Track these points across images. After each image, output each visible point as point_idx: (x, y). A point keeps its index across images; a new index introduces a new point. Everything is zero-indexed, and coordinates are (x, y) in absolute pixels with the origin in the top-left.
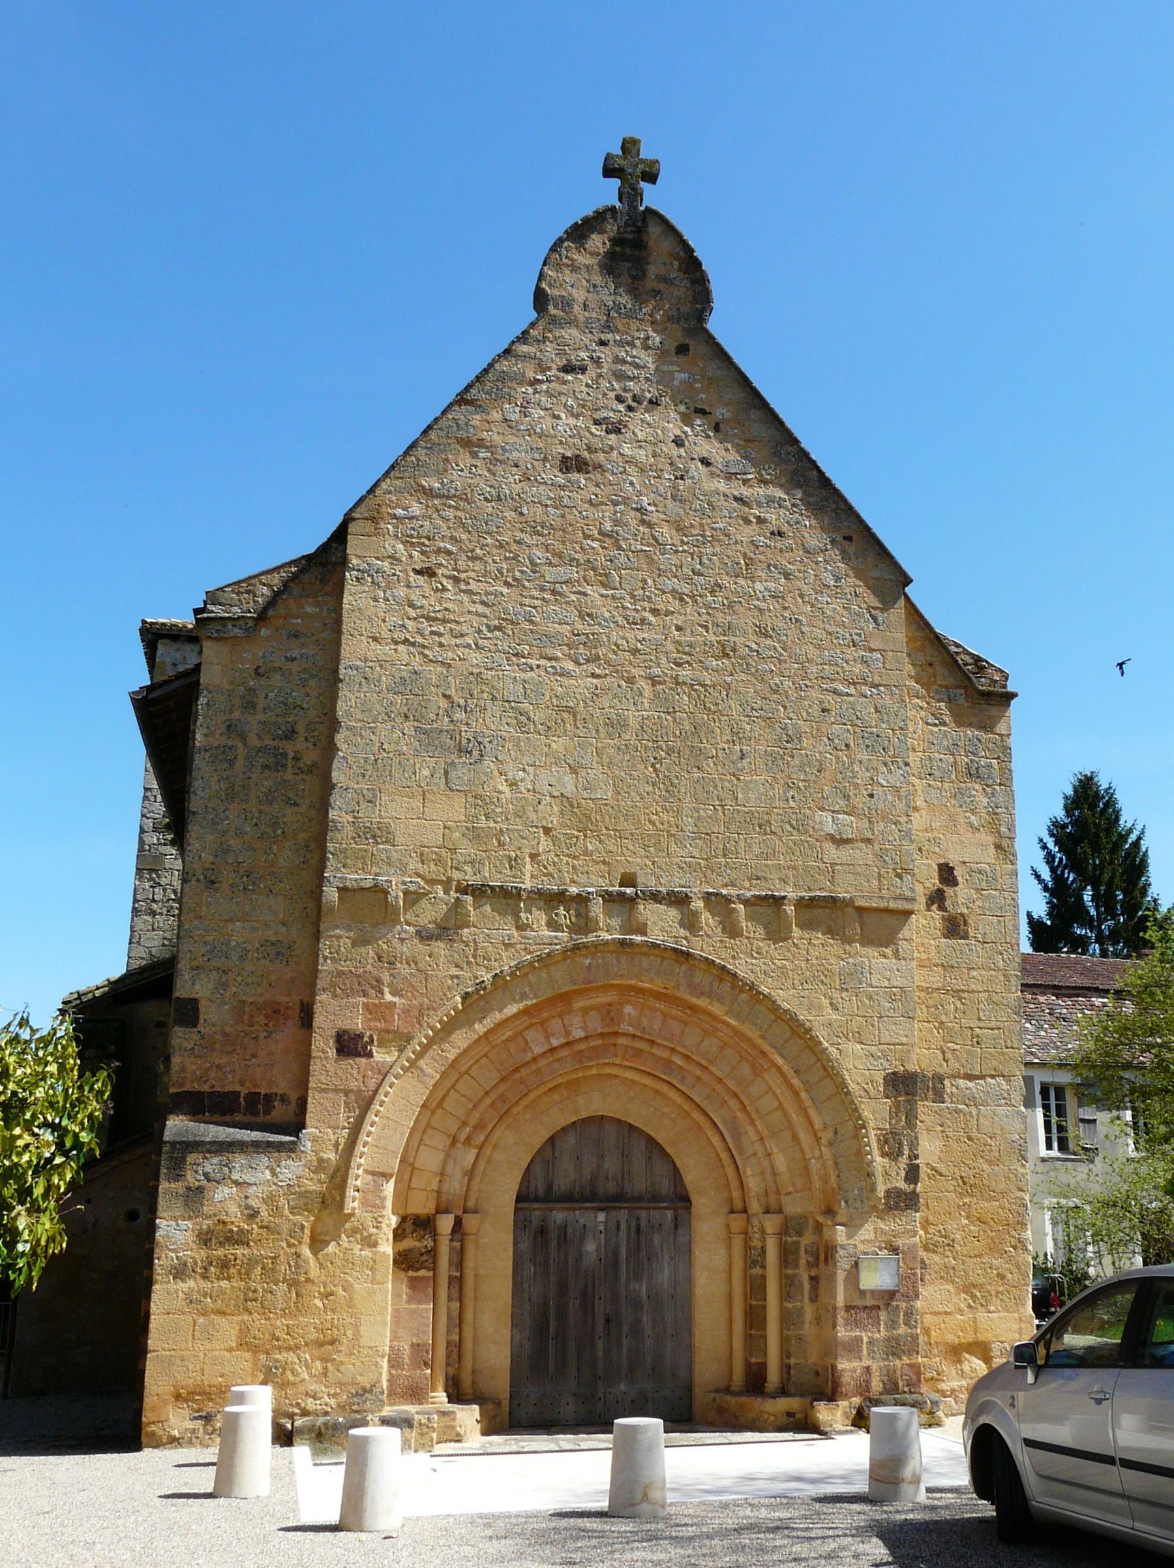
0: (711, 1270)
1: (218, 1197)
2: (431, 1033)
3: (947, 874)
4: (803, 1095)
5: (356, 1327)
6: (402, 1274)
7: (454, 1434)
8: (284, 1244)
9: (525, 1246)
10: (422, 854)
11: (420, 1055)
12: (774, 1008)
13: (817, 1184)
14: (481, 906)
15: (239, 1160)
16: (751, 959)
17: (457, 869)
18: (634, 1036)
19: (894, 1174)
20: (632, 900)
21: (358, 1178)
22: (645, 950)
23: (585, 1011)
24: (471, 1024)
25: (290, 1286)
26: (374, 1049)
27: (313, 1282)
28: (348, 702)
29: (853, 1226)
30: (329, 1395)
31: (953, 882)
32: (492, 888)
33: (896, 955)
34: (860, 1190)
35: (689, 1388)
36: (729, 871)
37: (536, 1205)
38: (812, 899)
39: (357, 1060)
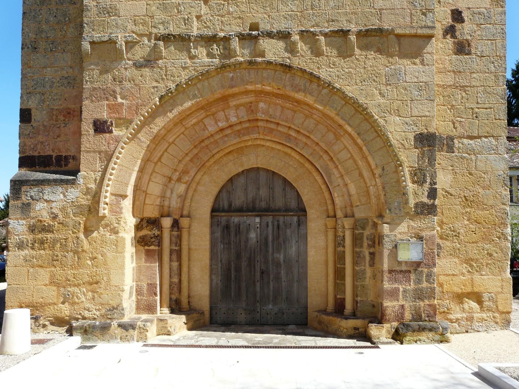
0: (317, 248)
1: (37, 208)
2: (142, 118)
3: (457, 16)
4: (364, 148)
5: (108, 275)
6: (142, 248)
7: (166, 331)
8: (71, 232)
9: (218, 234)
10: (135, 21)
11: (138, 130)
12: (344, 96)
13: (374, 200)
14: (168, 47)
15: (47, 189)
16: (329, 68)
17: (155, 27)
18: (267, 121)
19: (420, 193)
20: (256, 38)
21: (107, 197)
23: (237, 107)
25: (74, 253)
26: (113, 129)
27: (86, 252)
29: (394, 224)
30: (96, 310)
31: (462, 21)
32: (174, 36)
33: (422, 63)
34: (399, 203)
35: (306, 308)
36: (315, 18)
37: (223, 214)
38: (367, 31)
39: (104, 135)
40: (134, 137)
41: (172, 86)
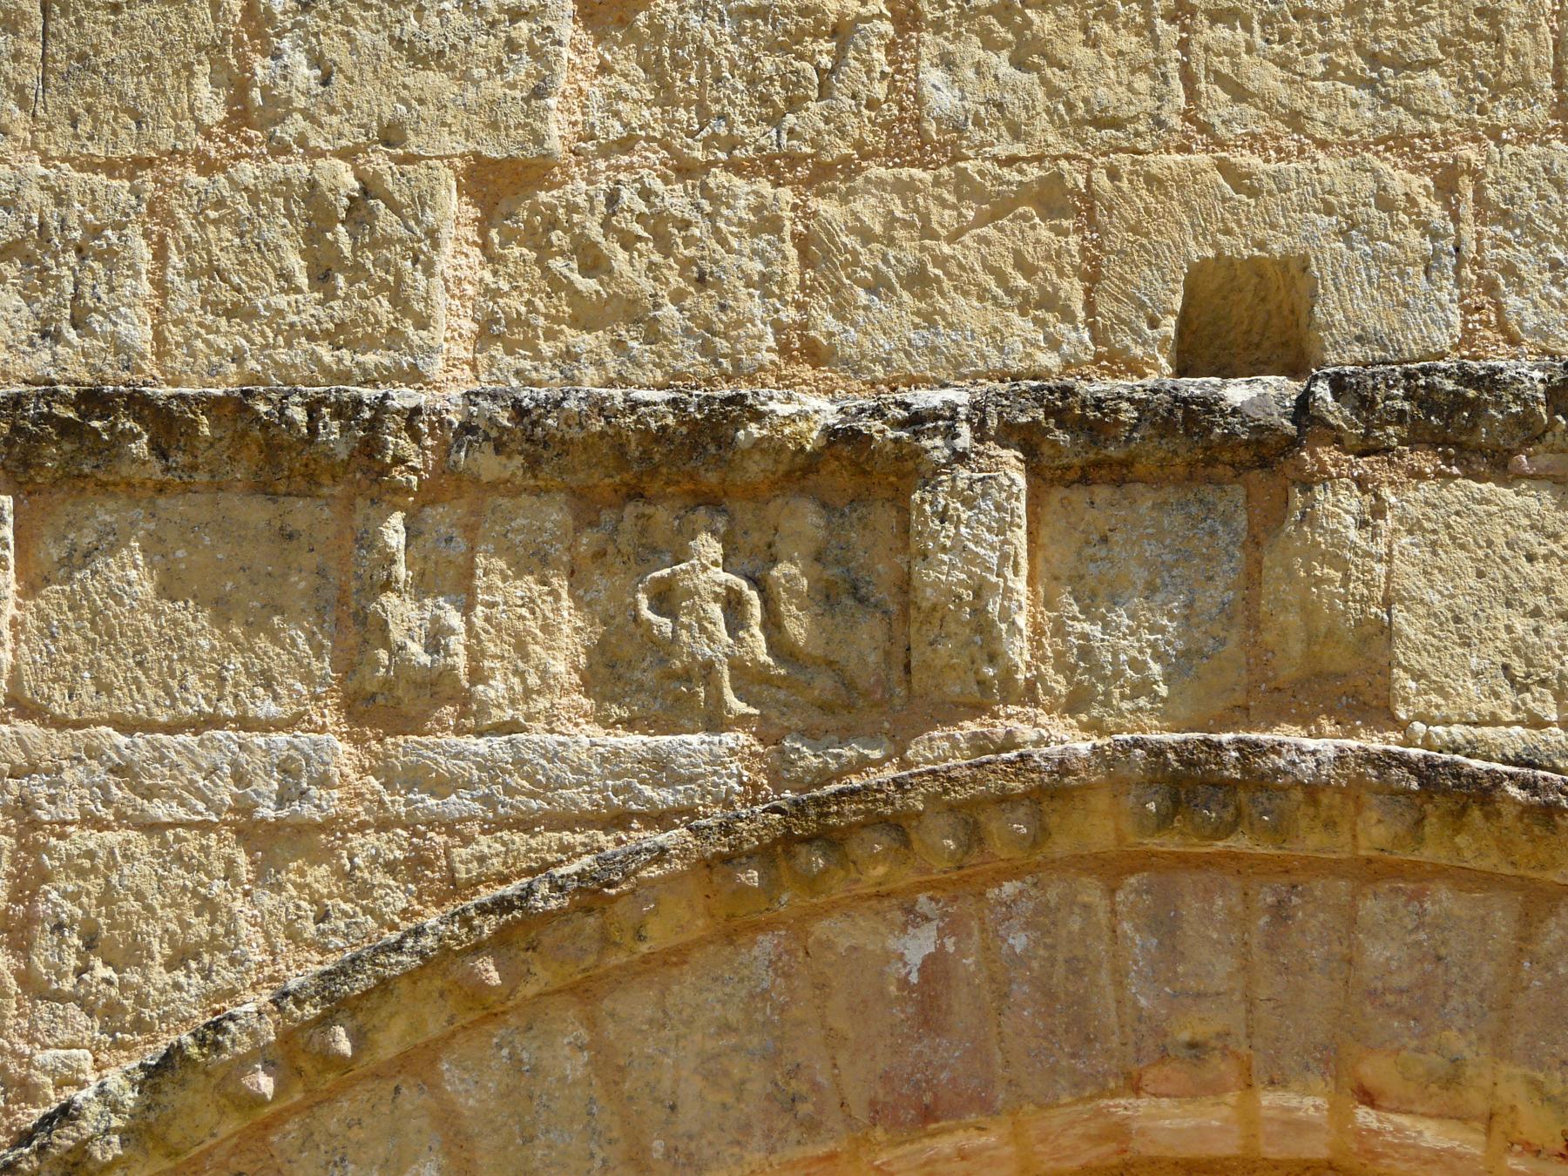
20: (1269, 460)
22: (1375, 831)
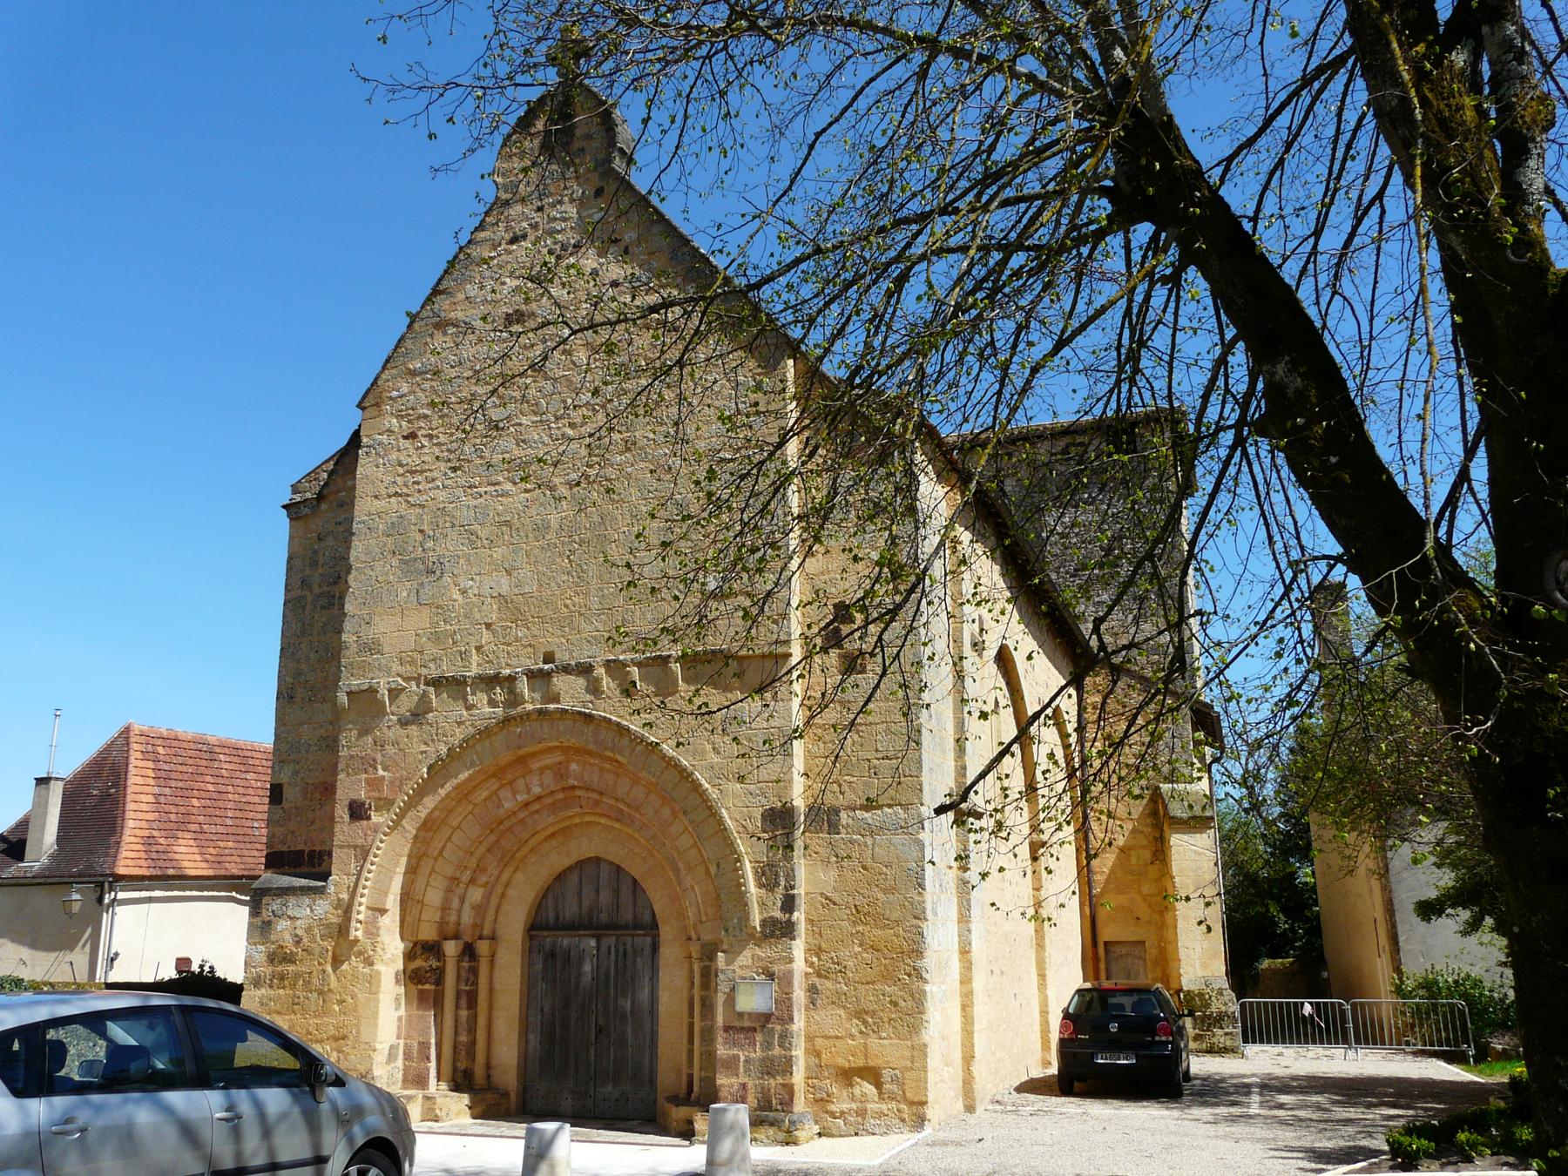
5: (358, 1026)
9: (539, 967)
11: (401, 816)
15: (292, 901)
21: (361, 912)
23: (542, 770)
24: (435, 791)
28: (358, 550)
29: (732, 954)
40: (397, 824)
41: (444, 750)
